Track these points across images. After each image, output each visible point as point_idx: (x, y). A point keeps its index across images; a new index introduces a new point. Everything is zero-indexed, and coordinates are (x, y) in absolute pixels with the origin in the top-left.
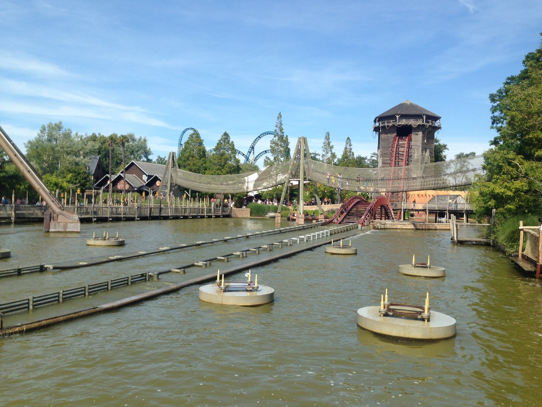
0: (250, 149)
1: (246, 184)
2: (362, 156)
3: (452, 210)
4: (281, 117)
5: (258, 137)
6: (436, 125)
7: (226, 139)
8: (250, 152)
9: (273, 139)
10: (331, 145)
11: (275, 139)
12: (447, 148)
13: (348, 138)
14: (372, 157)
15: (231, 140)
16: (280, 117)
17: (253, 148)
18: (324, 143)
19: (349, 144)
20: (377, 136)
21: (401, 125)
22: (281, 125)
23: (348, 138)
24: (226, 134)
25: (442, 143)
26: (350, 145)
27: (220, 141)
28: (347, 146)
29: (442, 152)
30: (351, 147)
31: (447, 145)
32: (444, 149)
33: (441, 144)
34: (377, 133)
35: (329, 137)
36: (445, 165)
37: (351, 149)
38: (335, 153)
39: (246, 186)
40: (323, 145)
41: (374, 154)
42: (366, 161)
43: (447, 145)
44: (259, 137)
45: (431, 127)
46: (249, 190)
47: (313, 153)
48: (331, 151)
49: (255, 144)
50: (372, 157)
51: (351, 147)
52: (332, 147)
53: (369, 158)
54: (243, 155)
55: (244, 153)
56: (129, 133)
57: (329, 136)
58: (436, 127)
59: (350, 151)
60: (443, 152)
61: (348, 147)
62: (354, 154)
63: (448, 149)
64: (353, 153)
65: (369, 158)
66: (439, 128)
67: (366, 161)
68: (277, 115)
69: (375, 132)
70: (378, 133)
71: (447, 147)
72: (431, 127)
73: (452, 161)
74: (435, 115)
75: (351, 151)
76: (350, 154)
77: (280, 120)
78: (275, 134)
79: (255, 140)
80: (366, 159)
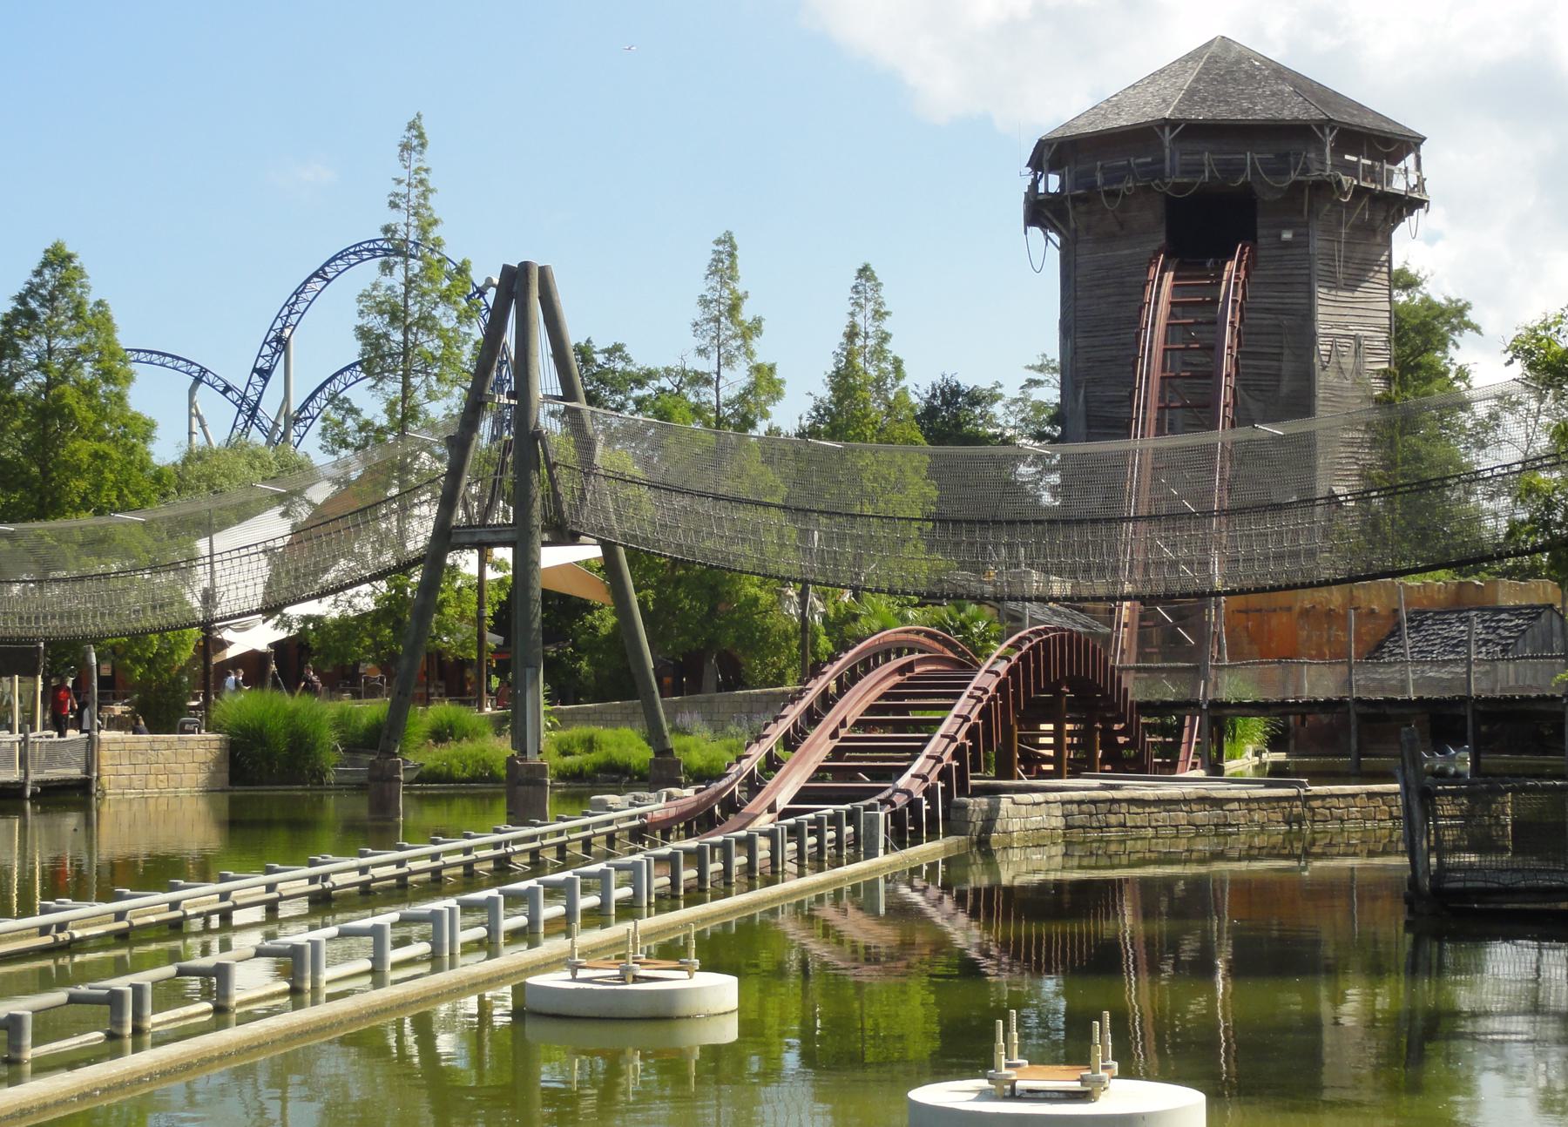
0: (267, 350)
1: (201, 572)
2: (967, 382)
3: (1494, 700)
4: (423, 145)
5: (316, 275)
6: (1399, 185)
7: (63, 286)
8: (265, 374)
9: (375, 286)
10: (747, 314)
11: (386, 281)
12: (1468, 325)
13: (865, 272)
14: (1033, 383)
15: (91, 299)
16: (415, 142)
17: (281, 344)
18: (705, 302)
19: (870, 306)
20: (1054, 255)
21: (1192, 185)
22: (424, 195)
23: (865, 272)
24: (57, 259)
25: (1439, 289)
26: (879, 315)
27: (21, 299)
28: (859, 320)
29: (1443, 343)
30: (887, 325)
31: (1467, 306)
32: (1453, 329)
33: (1438, 298)
34: (1053, 235)
35: (732, 267)
36: (1469, 425)
37: (885, 338)
38: (772, 369)
39: (198, 589)
40: (697, 313)
41: (1041, 369)
42: (998, 409)
43: (1467, 306)
44: (320, 274)
45: (1365, 200)
46: (218, 613)
47: (668, 372)
48: (750, 354)
49: (294, 318)
50: (1033, 383)
51: (887, 325)
52: (755, 328)
53: (1011, 391)
54: (227, 389)
55: (231, 383)
56: (938, 381)
57: (731, 255)
58: (1397, 197)
59: (879, 353)
60: (1452, 350)
61: (864, 322)
62: (905, 367)
63: (1477, 329)
64: (898, 364)
65: (1011, 391)
66: (1408, 204)
67: (998, 409)
68: (400, 134)
69: (1035, 231)
70: (1057, 239)
71: (1471, 316)
72: (1365, 200)
73: (1506, 401)
74: (1386, 127)
75: (883, 351)
76: (880, 370)
77: (414, 166)
78: (392, 249)
79: (297, 293)
80: (994, 398)
